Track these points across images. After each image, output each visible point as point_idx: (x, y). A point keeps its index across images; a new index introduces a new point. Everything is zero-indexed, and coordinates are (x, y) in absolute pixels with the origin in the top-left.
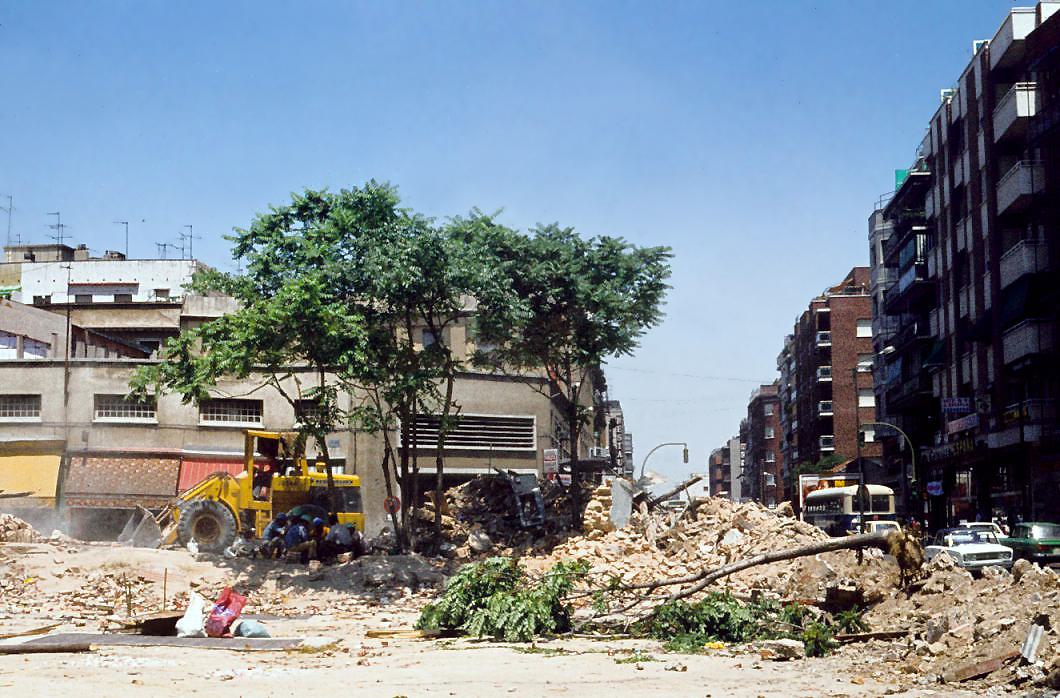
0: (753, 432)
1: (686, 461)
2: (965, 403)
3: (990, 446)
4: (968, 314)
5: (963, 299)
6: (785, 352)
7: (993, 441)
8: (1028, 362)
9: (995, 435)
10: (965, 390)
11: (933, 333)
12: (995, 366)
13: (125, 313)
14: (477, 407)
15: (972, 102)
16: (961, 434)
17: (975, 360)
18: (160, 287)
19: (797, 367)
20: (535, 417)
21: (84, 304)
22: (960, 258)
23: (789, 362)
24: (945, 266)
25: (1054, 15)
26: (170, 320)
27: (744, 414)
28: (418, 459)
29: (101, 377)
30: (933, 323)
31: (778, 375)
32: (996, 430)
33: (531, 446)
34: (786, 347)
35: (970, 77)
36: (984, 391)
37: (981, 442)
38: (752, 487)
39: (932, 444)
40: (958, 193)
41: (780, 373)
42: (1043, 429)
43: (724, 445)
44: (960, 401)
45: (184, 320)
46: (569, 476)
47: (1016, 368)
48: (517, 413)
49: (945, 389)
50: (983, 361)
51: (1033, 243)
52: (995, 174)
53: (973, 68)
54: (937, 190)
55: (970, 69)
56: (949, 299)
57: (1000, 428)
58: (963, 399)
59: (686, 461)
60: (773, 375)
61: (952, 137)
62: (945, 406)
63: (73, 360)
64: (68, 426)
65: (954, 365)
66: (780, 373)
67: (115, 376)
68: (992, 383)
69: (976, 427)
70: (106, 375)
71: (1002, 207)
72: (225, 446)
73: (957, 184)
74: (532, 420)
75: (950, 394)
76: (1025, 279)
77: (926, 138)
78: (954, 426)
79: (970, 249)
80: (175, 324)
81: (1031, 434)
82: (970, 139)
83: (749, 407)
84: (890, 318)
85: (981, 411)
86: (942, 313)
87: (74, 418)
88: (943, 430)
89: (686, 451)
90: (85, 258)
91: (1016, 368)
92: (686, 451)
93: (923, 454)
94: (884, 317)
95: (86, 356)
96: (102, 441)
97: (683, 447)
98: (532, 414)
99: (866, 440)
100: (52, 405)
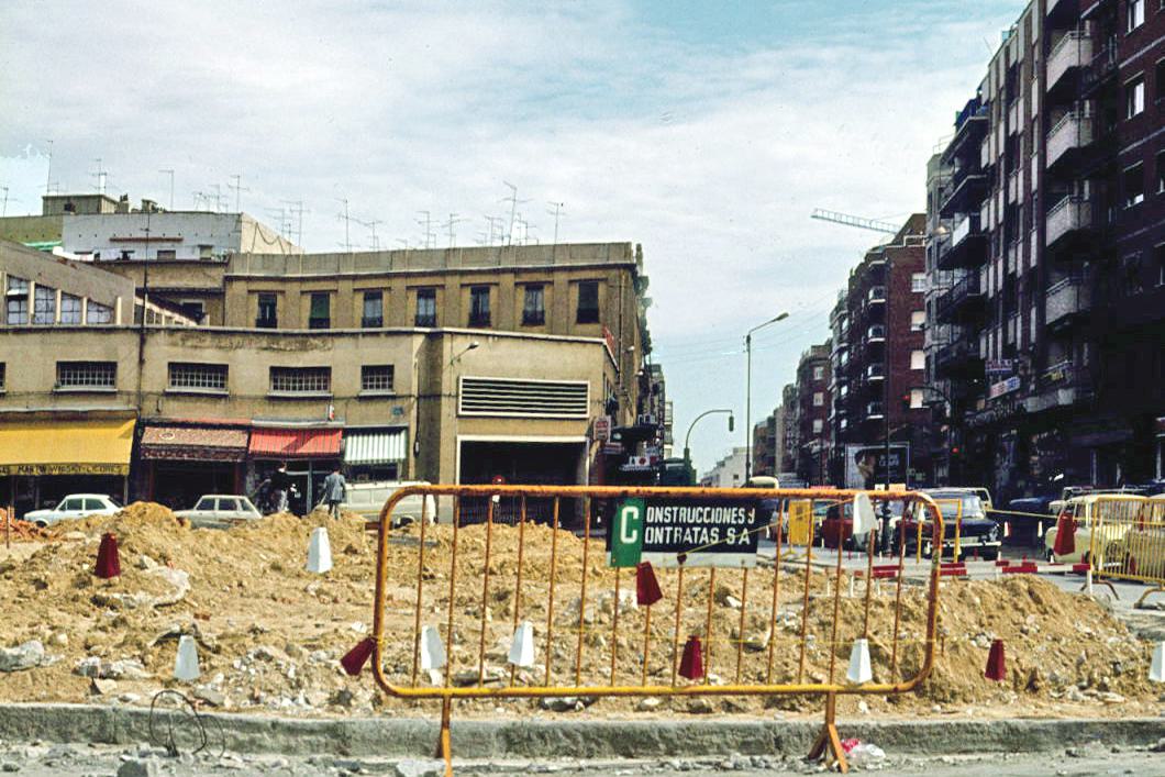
0: (801, 398)
1: (731, 429)
2: (1008, 365)
3: (1029, 410)
4: (1016, 270)
5: (1012, 254)
6: (838, 309)
7: (1031, 405)
8: (1067, 323)
9: (1034, 399)
10: (1009, 351)
11: (983, 290)
12: (1038, 325)
13: (169, 272)
14: (534, 373)
15: (1029, 47)
16: (1003, 398)
17: (1019, 320)
18: (204, 243)
19: (850, 326)
20: (588, 382)
21: (166, 263)
22: (1011, 210)
23: (841, 319)
24: (996, 218)
25: (1061, 157)
26: (215, 280)
27: (792, 379)
28: (253, 437)
29: (174, 344)
30: (983, 279)
31: (830, 334)
32: (1034, 394)
33: (585, 413)
34: (840, 302)
35: (1027, 20)
36: (1024, 351)
37: (1021, 406)
38: (797, 462)
39: (974, 408)
40: (1012, 141)
41: (831, 331)
42: (1077, 392)
43: (771, 414)
44: (1003, 362)
45: (229, 280)
46: (619, 444)
47: (1057, 328)
48: (572, 378)
49: (991, 349)
50: (1026, 322)
51: (1078, 201)
52: (1046, 123)
53: (1031, 12)
54: (992, 269)
55: (1027, 14)
56: (999, 255)
57: (1038, 393)
58: (1006, 361)
59: (731, 429)
60: (824, 335)
61: (1011, 79)
62: (990, 369)
63: (150, 326)
64: (141, 396)
65: (1000, 324)
66: (831, 331)
67: (189, 343)
68: (1034, 344)
69: (1016, 391)
70: (180, 343)
71: (1050, 161)
72: (293, 417)
73: (1011, 133)
74: (586, 386)
75: (995, 356)
76: (1069, 236)
77: (985, 80)
78: (996, 390)
79: (1020, 201)
80: (217, 284)
81: (1064, 397)
82: (1025, 86)
83: (799, 370)
84: (943, 273)
85: (1021, 372)
86: (992, 269)
87: (146, 388)
88: (988, 393)
89: (731, 419)
90: (747, 353)
91: (1057, 328)
92: (731, 419)
93: (967, 420)
94: (937, 271)
95: (223, 325)
96: (174, 410)
97: (728, 415)
98: (587, 379)
99: (912, 406)
100: (126, 377)
